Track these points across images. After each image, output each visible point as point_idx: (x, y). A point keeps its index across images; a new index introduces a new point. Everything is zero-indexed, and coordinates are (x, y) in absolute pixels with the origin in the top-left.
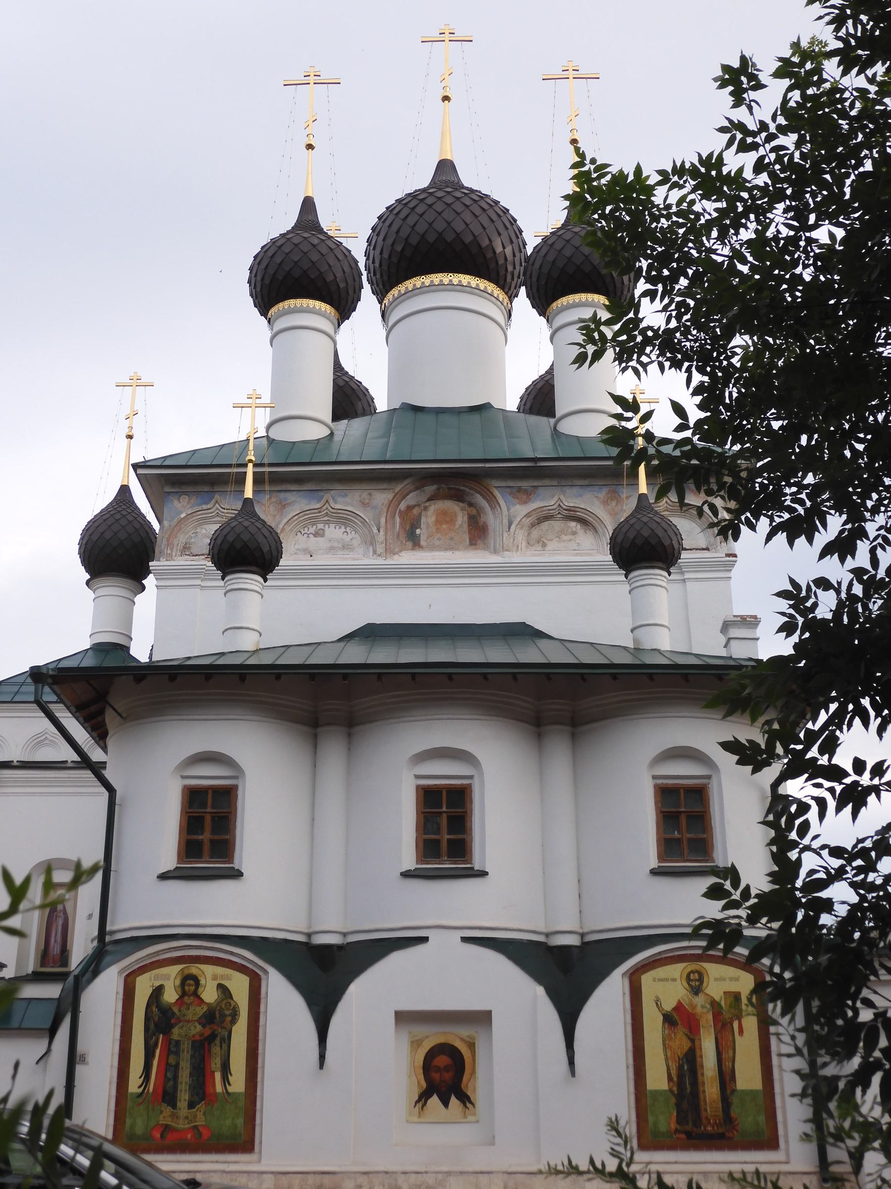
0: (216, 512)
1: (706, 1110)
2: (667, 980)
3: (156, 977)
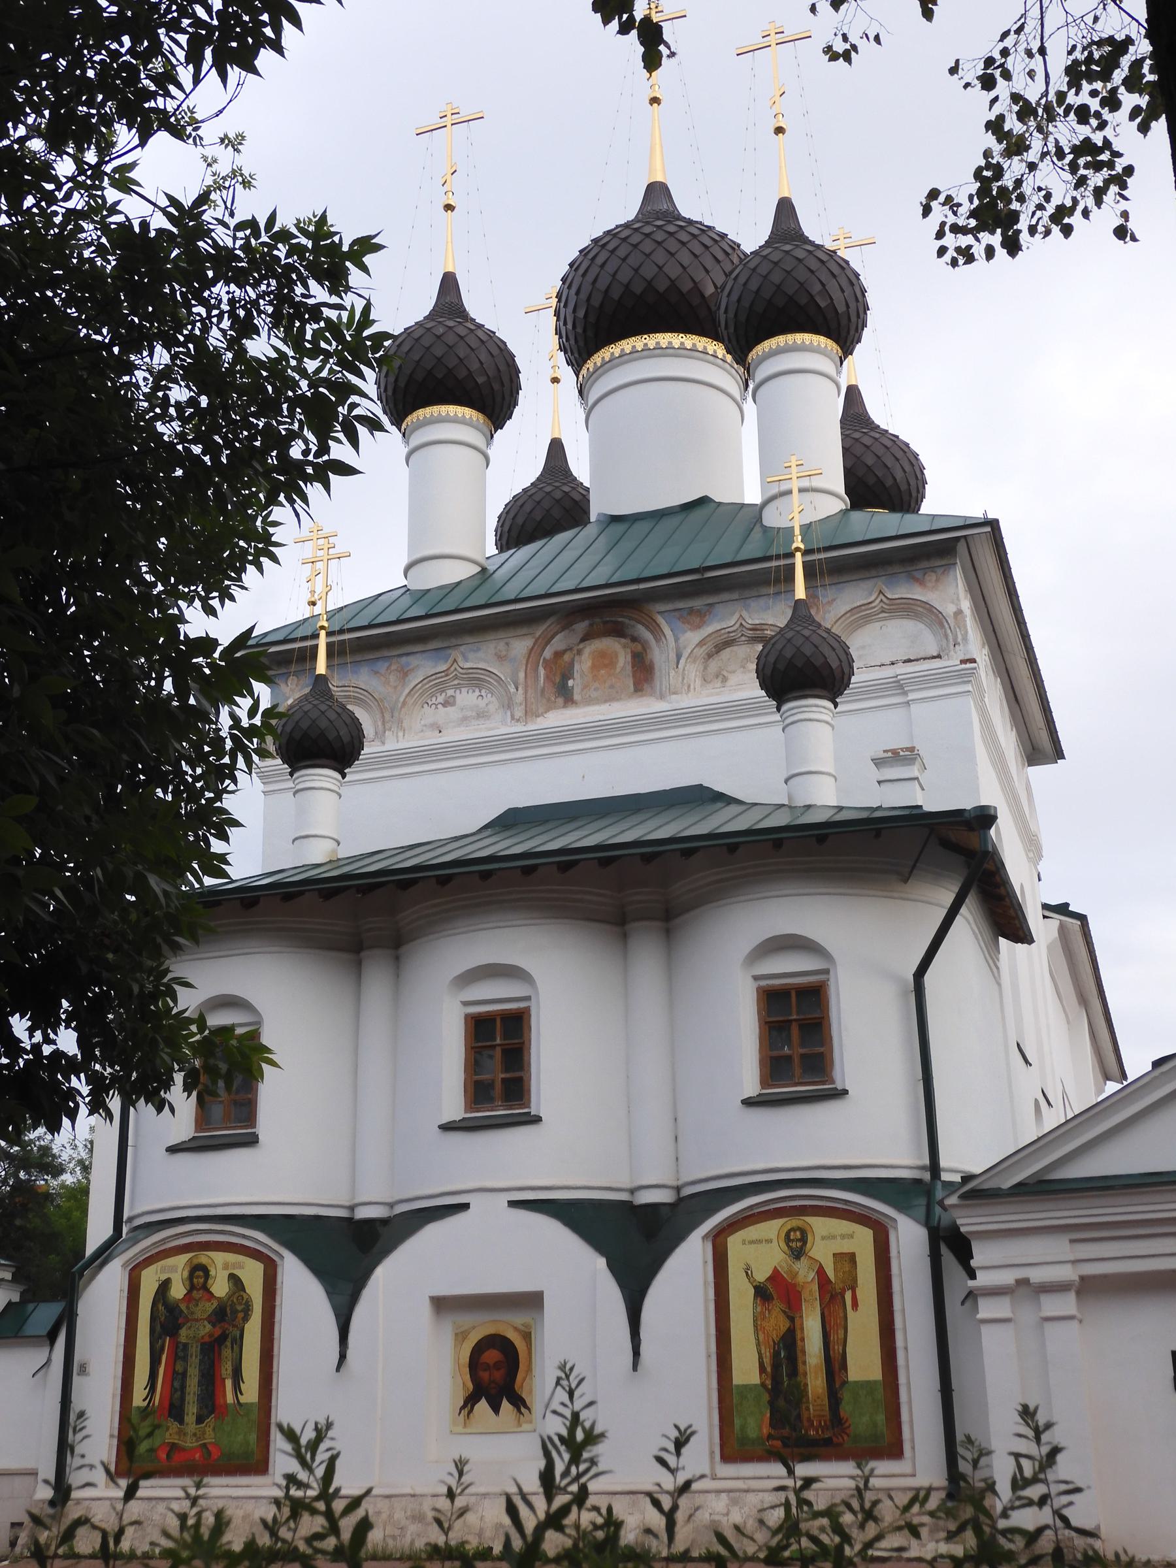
0: (880, 606)
1: (808, 1409)
2: (760, 1241)
3: (163, 1270)
